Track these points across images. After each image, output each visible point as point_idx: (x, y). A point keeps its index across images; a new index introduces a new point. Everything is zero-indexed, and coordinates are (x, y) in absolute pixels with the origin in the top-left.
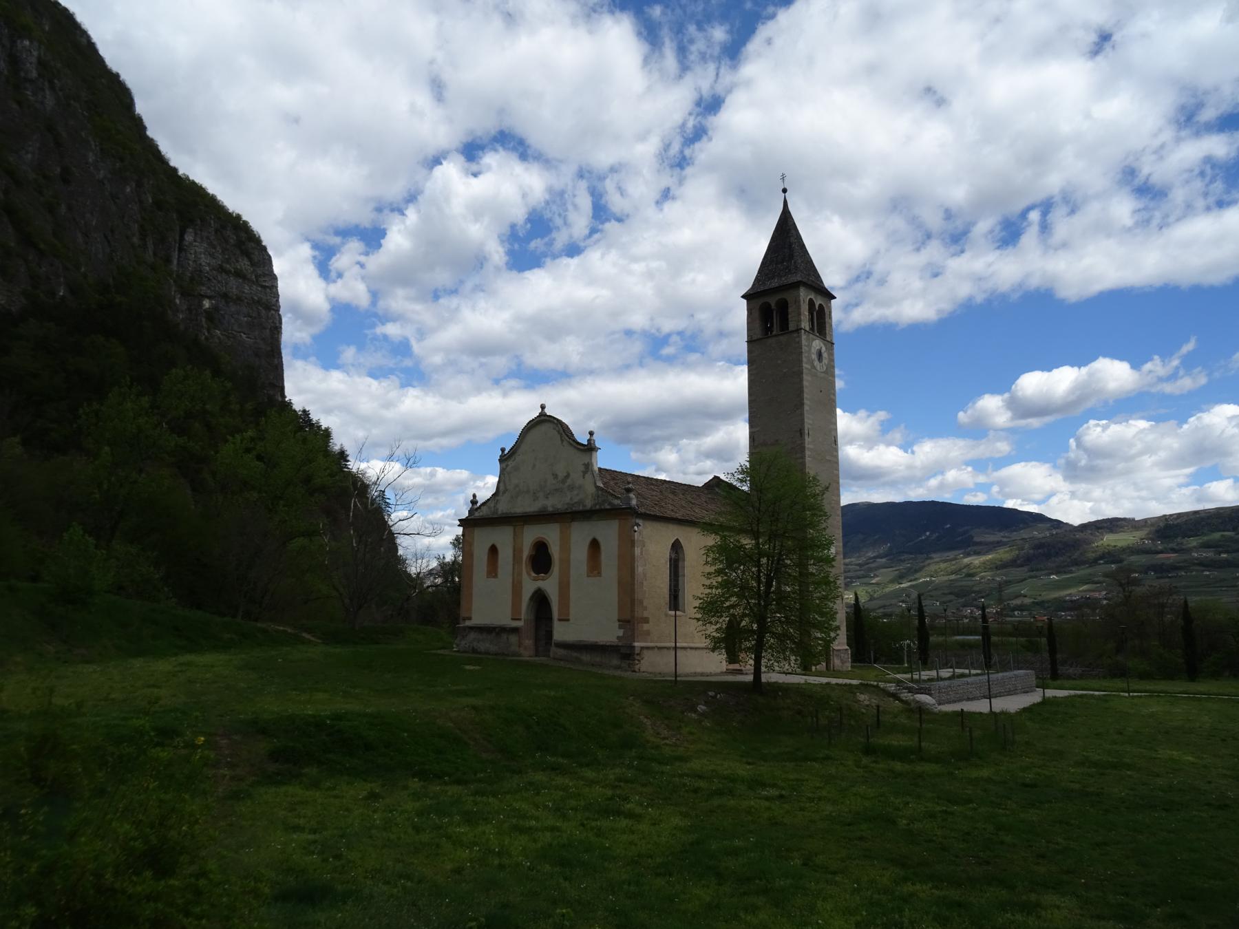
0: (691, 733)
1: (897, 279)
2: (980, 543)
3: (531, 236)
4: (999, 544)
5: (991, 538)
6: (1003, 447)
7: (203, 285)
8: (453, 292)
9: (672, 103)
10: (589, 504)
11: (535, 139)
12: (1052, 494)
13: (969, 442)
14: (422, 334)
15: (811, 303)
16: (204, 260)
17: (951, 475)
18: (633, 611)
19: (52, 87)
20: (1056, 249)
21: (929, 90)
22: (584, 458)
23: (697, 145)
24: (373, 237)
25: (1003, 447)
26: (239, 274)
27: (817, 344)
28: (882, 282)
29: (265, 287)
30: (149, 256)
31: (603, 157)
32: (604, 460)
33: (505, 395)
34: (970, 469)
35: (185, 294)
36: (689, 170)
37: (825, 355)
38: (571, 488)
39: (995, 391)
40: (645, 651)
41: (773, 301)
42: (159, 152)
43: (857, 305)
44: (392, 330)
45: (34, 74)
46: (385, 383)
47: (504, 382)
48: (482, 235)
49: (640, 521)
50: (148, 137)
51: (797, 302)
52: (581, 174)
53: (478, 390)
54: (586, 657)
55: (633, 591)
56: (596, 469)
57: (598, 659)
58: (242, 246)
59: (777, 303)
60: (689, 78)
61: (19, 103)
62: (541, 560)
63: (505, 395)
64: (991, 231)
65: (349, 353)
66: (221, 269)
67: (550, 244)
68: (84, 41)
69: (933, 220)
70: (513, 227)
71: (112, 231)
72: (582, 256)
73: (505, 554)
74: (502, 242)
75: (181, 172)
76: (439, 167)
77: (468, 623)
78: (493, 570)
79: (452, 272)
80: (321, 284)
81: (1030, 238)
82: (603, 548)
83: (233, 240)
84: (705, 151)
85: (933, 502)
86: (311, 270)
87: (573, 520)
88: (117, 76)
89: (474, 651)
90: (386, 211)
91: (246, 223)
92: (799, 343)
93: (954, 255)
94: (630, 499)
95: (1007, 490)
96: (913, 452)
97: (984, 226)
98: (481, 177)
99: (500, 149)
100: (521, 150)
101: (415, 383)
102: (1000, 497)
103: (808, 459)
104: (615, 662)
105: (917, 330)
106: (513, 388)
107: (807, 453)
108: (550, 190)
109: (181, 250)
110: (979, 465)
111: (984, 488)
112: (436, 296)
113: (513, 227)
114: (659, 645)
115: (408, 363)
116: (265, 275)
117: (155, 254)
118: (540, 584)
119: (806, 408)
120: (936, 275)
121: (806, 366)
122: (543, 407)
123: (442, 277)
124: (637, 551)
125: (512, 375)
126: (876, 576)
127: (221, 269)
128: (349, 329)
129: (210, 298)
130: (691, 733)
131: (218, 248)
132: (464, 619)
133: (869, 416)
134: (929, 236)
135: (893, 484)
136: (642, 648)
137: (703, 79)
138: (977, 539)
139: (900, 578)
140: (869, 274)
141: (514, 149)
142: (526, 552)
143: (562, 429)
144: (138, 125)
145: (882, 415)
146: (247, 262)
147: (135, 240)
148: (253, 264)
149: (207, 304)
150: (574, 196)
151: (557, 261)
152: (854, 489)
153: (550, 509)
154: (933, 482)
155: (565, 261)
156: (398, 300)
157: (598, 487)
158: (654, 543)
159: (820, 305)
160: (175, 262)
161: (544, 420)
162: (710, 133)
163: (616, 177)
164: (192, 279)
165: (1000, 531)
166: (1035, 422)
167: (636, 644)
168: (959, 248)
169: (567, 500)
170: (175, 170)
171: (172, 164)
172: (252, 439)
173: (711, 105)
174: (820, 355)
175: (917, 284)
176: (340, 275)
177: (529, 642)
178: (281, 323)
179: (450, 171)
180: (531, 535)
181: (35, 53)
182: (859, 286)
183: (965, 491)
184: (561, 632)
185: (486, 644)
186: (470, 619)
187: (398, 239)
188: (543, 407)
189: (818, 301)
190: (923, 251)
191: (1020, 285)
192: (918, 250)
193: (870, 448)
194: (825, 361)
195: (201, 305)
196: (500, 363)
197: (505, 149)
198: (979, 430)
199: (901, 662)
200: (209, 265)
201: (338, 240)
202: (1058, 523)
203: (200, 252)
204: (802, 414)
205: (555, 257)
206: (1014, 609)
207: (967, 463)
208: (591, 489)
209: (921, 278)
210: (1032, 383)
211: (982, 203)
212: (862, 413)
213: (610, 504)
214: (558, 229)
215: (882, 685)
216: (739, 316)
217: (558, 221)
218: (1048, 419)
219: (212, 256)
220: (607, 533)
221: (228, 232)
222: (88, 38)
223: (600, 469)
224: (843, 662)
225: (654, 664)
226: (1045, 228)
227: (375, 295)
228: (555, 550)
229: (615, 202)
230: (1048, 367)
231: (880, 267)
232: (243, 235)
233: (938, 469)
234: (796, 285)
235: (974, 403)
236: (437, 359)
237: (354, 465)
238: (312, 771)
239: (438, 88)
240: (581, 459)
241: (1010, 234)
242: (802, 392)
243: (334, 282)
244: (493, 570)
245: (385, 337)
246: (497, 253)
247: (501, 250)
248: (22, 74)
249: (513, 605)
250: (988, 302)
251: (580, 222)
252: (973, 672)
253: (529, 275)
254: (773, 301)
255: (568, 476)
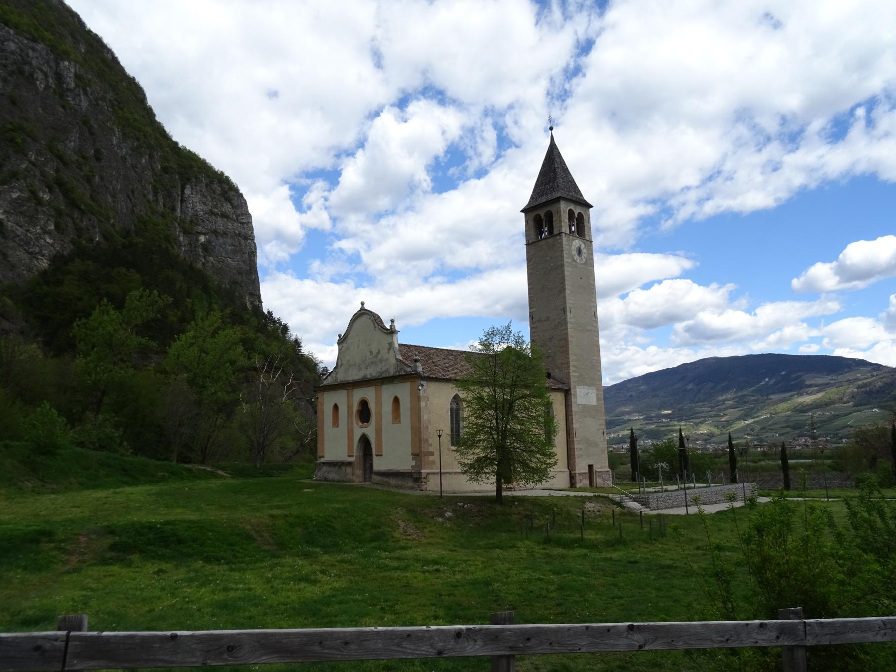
0: (431, 532)
1: (741, 175)
2: (811, 386)
3: (449, 165)
4: (827, 385)
5: (819, 381)
6: (834, 306)
7: (199, 225)
8: (392, 212)
9: (557, 47)
10: (392, 372)
11: (453, 90)
12: (874, 344)
13: (804, 304)
14: (369, 246)
15: (571, 213)
16: (199, 207)
17: (788, 331)
18: (420, 447)
19: (85, 93)
20: (879, 139)
21: (767, 15)
22: (387, 339)
23: (575, 81)
24: (332, 177)
25: (834, 306)
26: (224, 216)
27: (577, 243)
28: (730, 178)
29: (243, 223)
30: (160, 208)
31: (502, 99)
32: (401, 339)
33: (432, 289)
34: (805, 325)
35: (186, 232)
36: (569, 101)
37: (584, 251)
38: (381, 361)
39: (824, 261)
40: (430, 476)
41: (542, 213)
42: (165, 131)
43: (708, 199)
44: (346, 245)
45: (73, 85)
46: (344, 286)
47: (430, 279)
48: (414, 167)
49: (424, 383)
50: (156, 122)
51: (559, 212)
52: (486, 113)
53: (412, 286)
54: (393, 481)
55: (420, 432)
56: (397, 346)
57: (400, 482)
58: (224, 193)
59: (546, 214)
60: (569, 28)
61: (63, 107)
62: (364, 413)
63: (432, 289)
64: (824, 129)
65: (316, 265)
66: (211, 213)
67: (465, 169)
68: (110, 56)
69: (771, 125)
70: (437, 158)
71: (133, 192)
72: (487, 177)
73: (343, 410)
74: (428, 171)
75: (180, 145)
76: (378, 118)
77: (322, 460)
78: (336, 423)
79: (402, 196)
80: (296, 215)
81: (857, 131)
82: (401, 402)
83: (218, 190)
84: (580, 86)
85: (770, 354)
86: (290, 205)
87: (383, 383)
88: (134, 79)
89: (326, 479)
90: (343, 156)
91: (227, 178)
92: (561, 243)
93: (791, 151)
94: (416, 367)
95: (836, 341)
96: (755, 315)
97: (817, 124)
98: (409, 122)
99: (422, 97)
100: (440, 97)
101: (365, 284)
102: (830, 347)
103: (569, 330)
104: (410, 484)
105: (759, 216)
106: (439, 283)
107: (569, 325)
108: (463, 128)
109: (182, 201)
110: (813, 322)
111: (813, 340)
112: (379, 216)
113: (437, 158)
114: (451, 471)
115: (359, 269)
116: (243, 214)
117: (164, 206)
118: (364, 430)
119: (567, 292)
120: (775, 170)
121: (567, 260)
122: (363, 304)
123: (384, 203)
124: (423, 404)
125: (434, 274)
126: (725, 415)
127: (211, 213)
128: (315, 248)
129: (204, 234)
130: (431, 532)
131: (209, 198)
132: (321, 457)
133: (720, 288)
134: (769, 139)
135: (740, 341)
136: (428, 474)
137: (580, 25)
138: (807, 383)
139: (744, 417)
140: (719, 172)
141: (432, 97)
142: (356, 407)
143: (375, 319)
144: (149, 113)
145: (731, 286)
146: (229, 206)
147: (151, 197)
148: (233, 207)
149: (202, 239)
150: (482, 131)
151: (468, 183)
152: (707, 347)
153: (369, 377)
154: (772, 338)
155: (473, 182)
156: (353, 222)
157: (397, 360)
158: (438, 400)
159: (580, 214)
160: (179, 210)
161: (363, 313)
162: (584, 70)
163: (512, 111)
164: (191, 221)
165: (828, 375)
166: (859, 284)
167: (423, 471)
168: (795, 146)
169: (379, 370)
170: (176, 144)
171: (174, 139)
172: (194, 337)
173: (585, 47)
174: (579, 251)
175: (759, 178)
176: (309, 208)
177: (359, 472)
178: (256, 249)
179: (388, 118)
180: (359, 394)
181: (73, 70)
182: (711, 185)
183: (800, 343)
184: (379, 464)
185: (333, 475)
186: (323, 457)
187: (352, 175)
188: (363, 304)
189: (577, 210)
190: (764, 151)
191: (848, 172)
192: (760, 150)
193: (721, 314)
194: (584, 255)
195: (198, 240)
196: (429, 265)
197: (425, 98)
198: (812, 293)
199: (657, 479)
200: (202, 210)
201: (309, 181)
202: (878, 367)
203: (196, 201)
204: (565, 297)
205: (467, 179)
206: (842, 438)
207: (803, 321)
208: (393, 361)
209: (762, 173)
210: (858, 252)
211: (814, 107)
212: (714, 285)
213: (405, 371)
214: (470, 158)
215: (610, 496)
216: (520, 223)
217: (471, 152)
218: (872, 280)
219: (204, 203)
220: (403, 391)
221: (215, 186)
222: (112, 54)
223: (401, 345)
224: (604, 480)
225: (432, 485)
226: (870, 123)
227: (334, 220)
228: (372, 406)
229: (514, 132)
230: (871, 237)
231: (728, 166)
232: (226, 186)
233: (777, 326)
234: (557, 200)
235: (806, 272)
236: (381, 265)
237: (306, 350)
238: (135, 557)
239: (378, 59)
240: (386, 339)
241: (838, 130)
242: (564, 280)
243: (305, 212)
244: (336, 423)
245: (341, 250)
246: (424, 179)
247: (428, 179)
248: (65, 86)
249: (349, 445)
250: (820, 189)
251: (487, 152)
252: (697, 485)
253: (445, 195)
254: (542, 213)
255: (379, 352)
